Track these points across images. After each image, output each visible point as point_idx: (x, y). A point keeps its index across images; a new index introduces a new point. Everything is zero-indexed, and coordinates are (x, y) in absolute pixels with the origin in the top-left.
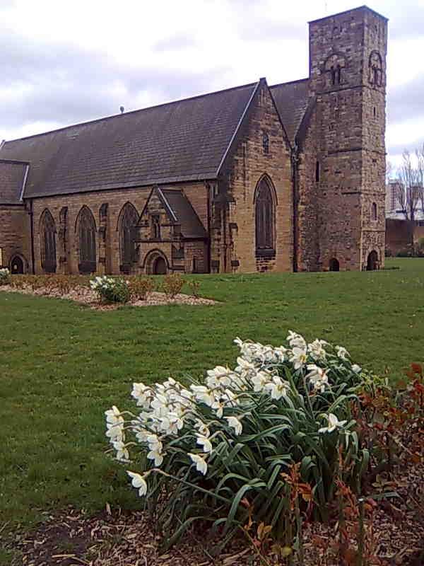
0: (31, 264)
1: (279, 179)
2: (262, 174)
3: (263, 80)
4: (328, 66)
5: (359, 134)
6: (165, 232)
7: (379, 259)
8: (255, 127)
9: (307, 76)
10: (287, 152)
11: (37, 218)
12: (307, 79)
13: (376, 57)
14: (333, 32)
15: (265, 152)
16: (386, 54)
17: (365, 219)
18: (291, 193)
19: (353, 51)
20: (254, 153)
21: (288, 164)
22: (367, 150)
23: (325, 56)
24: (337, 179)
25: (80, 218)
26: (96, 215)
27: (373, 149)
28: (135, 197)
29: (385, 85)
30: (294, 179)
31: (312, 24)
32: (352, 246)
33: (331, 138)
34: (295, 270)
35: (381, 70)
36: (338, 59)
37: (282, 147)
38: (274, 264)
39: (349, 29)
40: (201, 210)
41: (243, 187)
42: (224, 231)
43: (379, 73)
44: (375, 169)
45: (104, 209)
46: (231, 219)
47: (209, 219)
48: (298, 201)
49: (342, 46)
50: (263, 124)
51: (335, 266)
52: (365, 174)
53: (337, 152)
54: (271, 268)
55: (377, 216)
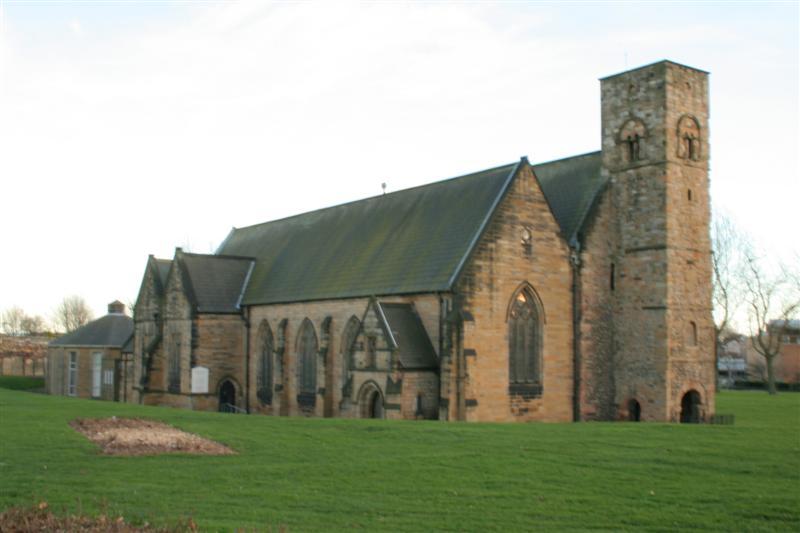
0: (244, 391)
1: (549, 289)
2: (520, 282)
3: (524, 161)
4: (624, 136)
5: (663, 227)
6: (382, 358)
7: (703, 401)
8: (509, 221)
9: (597, 147)
10: (563, 252)
11: (254, 331)
12: (598, 153)
13: (689, 123)
14: (629, 92)
15: (526, 253)
16: (707, 118)
17: (676, 344)
18: (569, 307)
19: (653, 117)
20: (507, 256)
21: (565, 268)
22: (676, 248)
23: (620, 122)
24: (637, 289)
25: (301, 335)
26: (318, 330)
27: (687, 246)
28: (358, 308)
29: (707, 158)
30: (575, 288)
31: (604, 81)
32: (655, 383)
33: (628, 232)
34: (576, 417)
35: (699, 140)
36: (637, 126)
37: (555, 245)
38: (539, 404)
39: (649, 89)
40: (432, 329)
41: (488, 300)
42: (458, 360)
43: (696, 143)
44: (692, 274)
45: (328, 324)
46: (467, 344)
47: (441, 342)
48: (580, 319)
49: (640, 110)
50: (522, 216)
51: (635, 411)
52: (674, 282)
53: (634, 251)
54: (535, 410)
55: (699, 339)
